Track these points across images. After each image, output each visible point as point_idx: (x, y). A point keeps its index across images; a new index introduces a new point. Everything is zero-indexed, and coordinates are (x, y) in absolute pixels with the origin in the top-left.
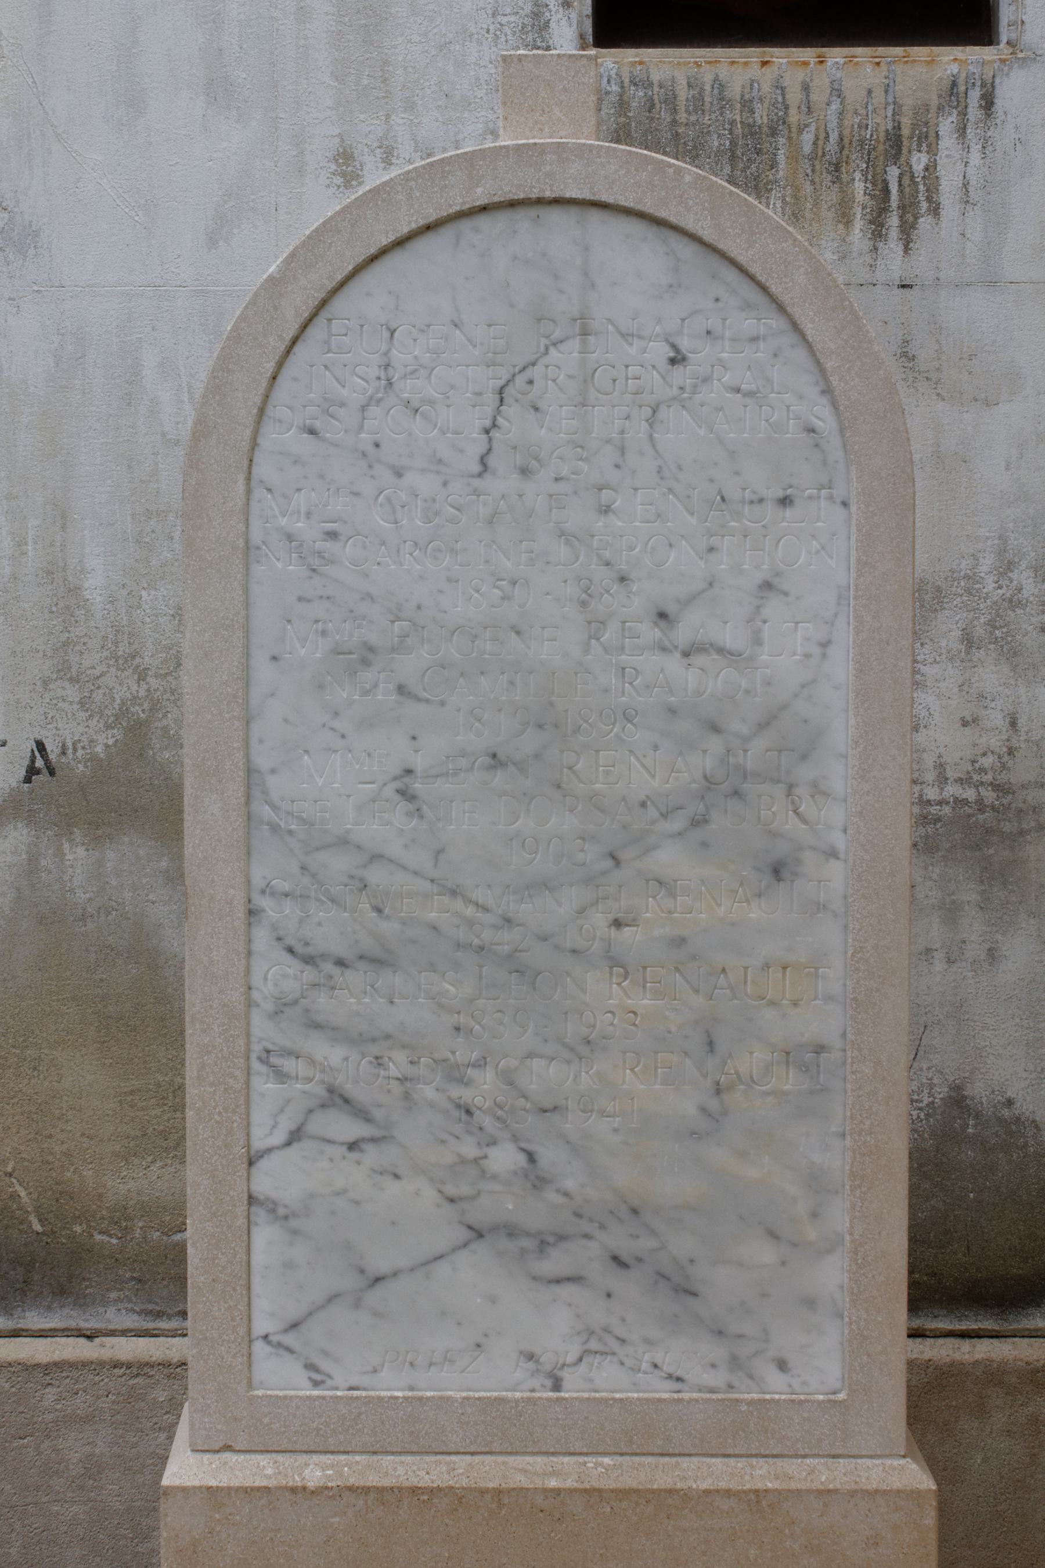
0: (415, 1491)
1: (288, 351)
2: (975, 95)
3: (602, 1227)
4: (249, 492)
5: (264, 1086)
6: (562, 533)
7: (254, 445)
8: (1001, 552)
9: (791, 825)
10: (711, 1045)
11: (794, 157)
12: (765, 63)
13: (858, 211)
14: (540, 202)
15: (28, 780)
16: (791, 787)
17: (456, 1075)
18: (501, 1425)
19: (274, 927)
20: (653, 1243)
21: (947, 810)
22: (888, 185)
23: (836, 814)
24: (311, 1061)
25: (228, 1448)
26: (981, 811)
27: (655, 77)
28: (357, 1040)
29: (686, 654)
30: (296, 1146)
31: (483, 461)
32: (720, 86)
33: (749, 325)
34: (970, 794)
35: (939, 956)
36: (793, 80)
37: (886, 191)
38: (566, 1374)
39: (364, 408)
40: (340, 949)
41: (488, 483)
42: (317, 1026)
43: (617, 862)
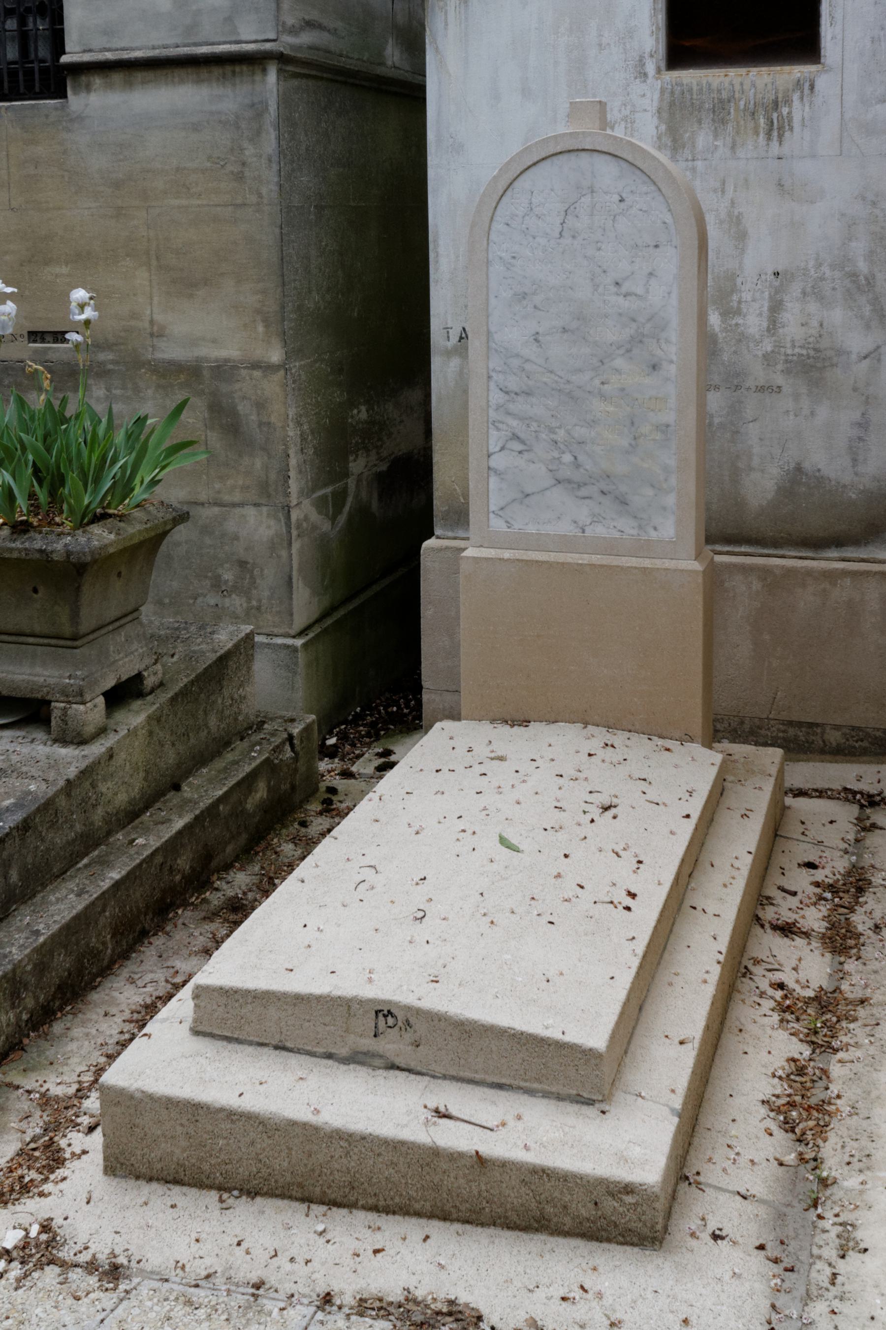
0: (537, 561)
1: (500, 199)
2: (807, 86)
3: (598, 481)
4: (488, 244)
5: (493, 433)
6: (585, 257)
7: (490, 229)
8: (817, 259)
9: (659, 352)
10: (633, 423)
11: (737, 109)
12: (726, 75)
13: (761, 130)
14: (578, 150)
15: (460, 341)
16: (658, 340)
17: (552, 430)
18: (566, 543)
19: (496, 382)
20: (614, 487)
21: (795, 358)
22: (774, 120)
23: (673, 349)
24: (508, 425)
25: (482, 546)
26: (809, 358)
27: (685, 83)
28: (522, 419)
29: (625, 296)
30: (502, 452)
31: (560, 233)
32: (709, 85)
33: (645, 189)
34: (804, 352)
35: (792, 413)
36: (737, 82)
37: (772, 122)
38: (586, 528)
39: (523, 217)
40: (516, 390)
41: (561, 241)
42: (509, 414)
43: (603, 363)
